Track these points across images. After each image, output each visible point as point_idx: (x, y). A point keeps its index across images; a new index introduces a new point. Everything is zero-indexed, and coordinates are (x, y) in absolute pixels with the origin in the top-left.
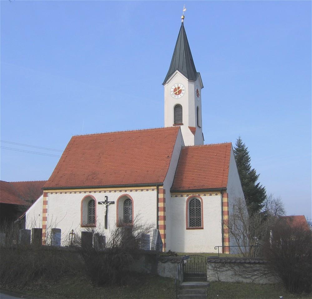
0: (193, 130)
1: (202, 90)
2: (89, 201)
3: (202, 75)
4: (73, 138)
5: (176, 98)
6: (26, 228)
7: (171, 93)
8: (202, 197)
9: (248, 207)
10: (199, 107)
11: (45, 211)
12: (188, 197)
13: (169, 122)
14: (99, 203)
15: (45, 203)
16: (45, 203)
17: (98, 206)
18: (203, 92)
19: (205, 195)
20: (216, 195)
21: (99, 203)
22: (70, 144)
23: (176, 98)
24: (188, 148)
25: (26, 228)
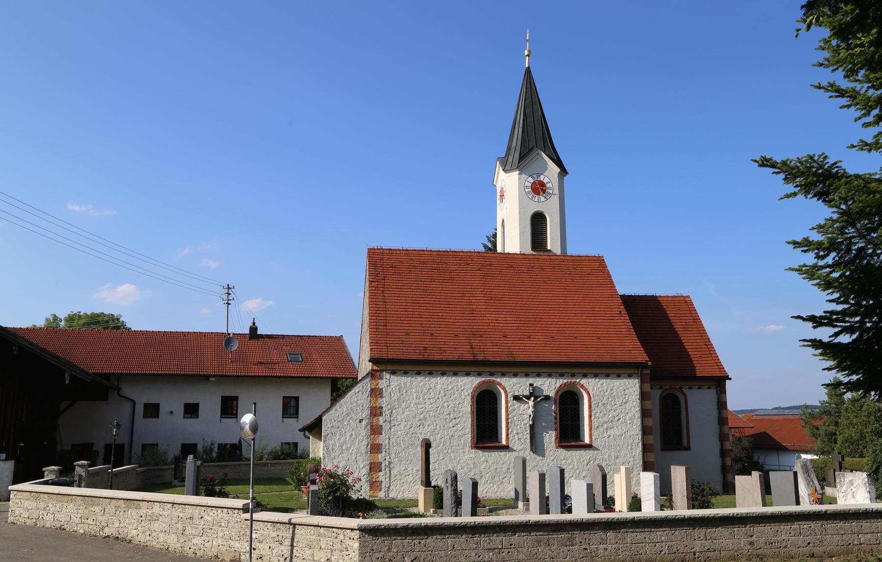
7: (527, 190)
14: (516, 398)
19: (690, 388)
20: (709, 388)
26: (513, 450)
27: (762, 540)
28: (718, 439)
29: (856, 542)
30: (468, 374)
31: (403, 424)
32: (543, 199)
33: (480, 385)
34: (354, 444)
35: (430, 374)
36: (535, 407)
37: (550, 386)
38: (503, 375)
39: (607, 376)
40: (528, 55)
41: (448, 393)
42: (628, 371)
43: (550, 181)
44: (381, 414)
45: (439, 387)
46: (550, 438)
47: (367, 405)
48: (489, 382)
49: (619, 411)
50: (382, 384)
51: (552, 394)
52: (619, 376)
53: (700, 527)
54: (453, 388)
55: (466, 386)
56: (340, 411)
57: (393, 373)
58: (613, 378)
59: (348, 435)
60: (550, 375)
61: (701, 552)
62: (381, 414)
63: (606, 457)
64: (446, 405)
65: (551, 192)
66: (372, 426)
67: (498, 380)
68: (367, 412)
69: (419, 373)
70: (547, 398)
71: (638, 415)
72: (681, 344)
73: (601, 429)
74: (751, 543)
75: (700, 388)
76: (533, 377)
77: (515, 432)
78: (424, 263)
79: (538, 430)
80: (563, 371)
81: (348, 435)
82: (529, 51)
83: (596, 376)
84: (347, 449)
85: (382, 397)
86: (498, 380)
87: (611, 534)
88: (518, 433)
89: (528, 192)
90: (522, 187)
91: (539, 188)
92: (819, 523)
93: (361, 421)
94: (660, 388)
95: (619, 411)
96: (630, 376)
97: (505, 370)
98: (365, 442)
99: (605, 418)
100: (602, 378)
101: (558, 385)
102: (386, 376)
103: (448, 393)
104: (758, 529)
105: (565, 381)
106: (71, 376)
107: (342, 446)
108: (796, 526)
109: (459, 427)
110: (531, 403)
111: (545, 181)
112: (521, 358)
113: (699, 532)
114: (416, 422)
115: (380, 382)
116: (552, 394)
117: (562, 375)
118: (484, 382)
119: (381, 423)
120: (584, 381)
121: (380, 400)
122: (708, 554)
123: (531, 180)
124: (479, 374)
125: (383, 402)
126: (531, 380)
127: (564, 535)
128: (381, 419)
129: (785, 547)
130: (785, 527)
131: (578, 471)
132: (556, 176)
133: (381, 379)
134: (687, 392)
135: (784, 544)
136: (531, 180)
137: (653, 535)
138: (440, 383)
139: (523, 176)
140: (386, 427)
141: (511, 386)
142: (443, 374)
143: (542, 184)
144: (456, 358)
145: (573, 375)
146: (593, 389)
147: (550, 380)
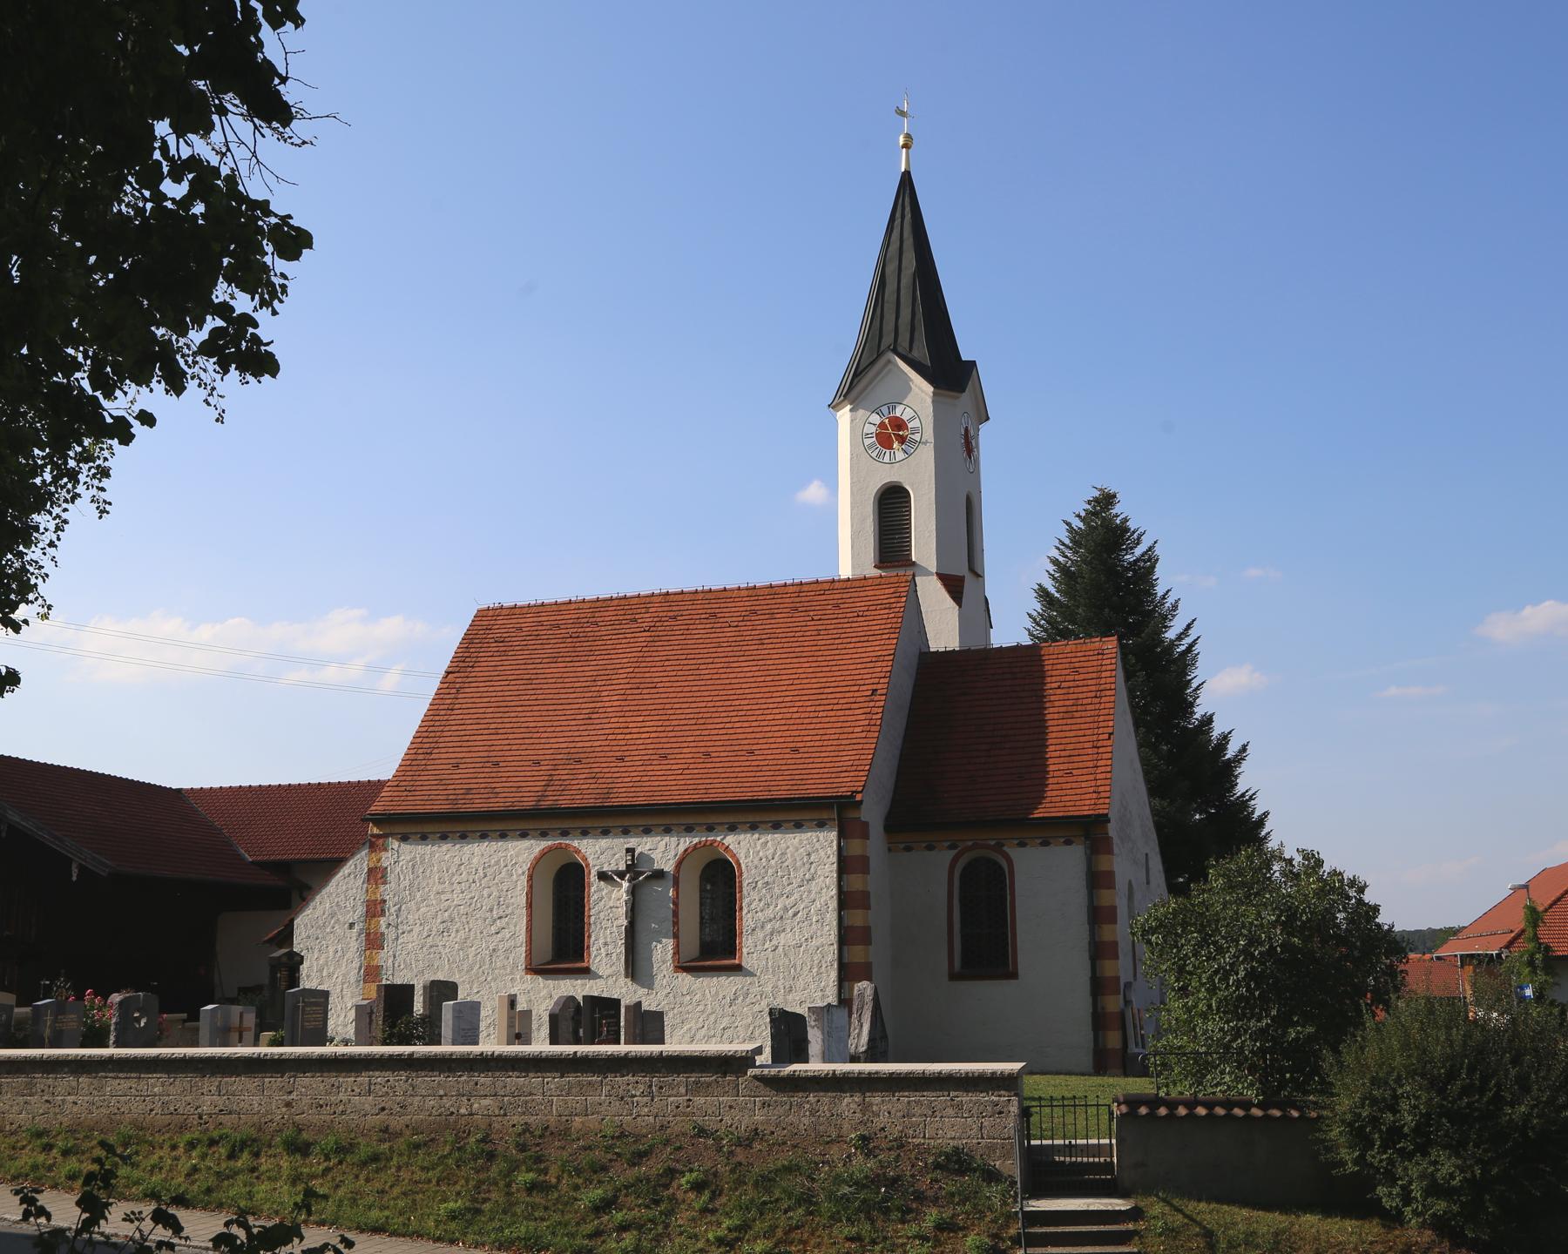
0: (953, 586)
1: (984, 428)
2: (552, 876)
3: (987, 376)
4: (482, 615)
5: (887, 459)
6: (1111, 644)
7: (868, 442)
8: (1016, 853)
9: (1157, 802)
10: (974, 500)
11: (375, 909)
12: (954, 852)
13: (849, 555)
14: (603, 876)
15: (376, 875)
16: (376, 875)
17: (595, 888)
18: (987, 436)
19: (1022, 845)
20: (1068, 842)
21: (603, 876)
22: (469, 640)
23: (887, 459)
24: (945, 658)
25: (1111, 644)
26: (597, 976)
27: (306, 1100)
28: (1086, 956)
29: (463, 1111)
30: (524, 835)
31: (417, 929)
32: (900, 455)
33: (544, 854)
34: (340, 966)
35: (463, 837)
36: (633, 892)
37: (664, 850)
38: (585, 833)
39: (776, 827)
40: (906, 146)
41: (490, 871)
42: (816, 815)
43: (917, 415)
44: (383, 913)
45: (475, 860)
46: (662, 952)
47: (362, 896)
48: (559, 847)
49: (796, 896)
50: (387, 859)
51: (669, 867)
52: (798, 826)
53: (213, 1074)
54: (497, 863)
55: (522, 852)
56: (319, 912)
57: (404, 838)
58: (788, 831)
59: (331, 950)
60: (667, 831)
61: (210, 1115)
62: (383, 913)
63: (769, 989)
64: (485, 893)
65: (917, 437)
66: (368, 935)
67: (575, 843)
68: (361, 910)
69: (444, 837)
70: (659, 875)
71: (834, 904)
72: (1042, 745)
73: (760, 934)
74: (288, 1105)
75: (1045, 843)
76: (637, 835)
77: (601, 941)
78: (558, 626)
79: (642, 937)
80: (690, 820)
81: (331, 950)
82: (908, 136)
83: (753, 827)
84: (330, 976)
85: (385, 883)
86: (575, 843)
87: (84, 1080)
88: (606, 944)
89: (870, 446)
90: (857, 436)
91: (892, 434)
92: (403, 1075)
93: (351, 926)
94: (952, 847)
95: (796, 896)
96: (821, 825)
97: (588, 824)
98: (356, 964)
99: (769, 912)
100: (766, 831)
101: (681, 849)
102: (394, 844)
103: (490, 871)
104: (304, 1080)
105: (696, 840)
106: (82, 868)
107: (321, 971)
108: (363, 1079)
109: (506, 934)
110: (625, 884)
111: (905, 418)
112: (621, 798)
113: (210, 1083)
114: (436, 925)
115: (384, 855)
116: (669, 867)
117: (689, 829)
118: (550, 850)
119: (383, 929)
120: (730, 840)
121: (382, 888)
122: (222, 1118)
123: (876, 419)
124: (544, 834)
125: (387, 892)
126: (632, 842)
127: (22, 1079)
128: (383, 921)
129: (343, 1113)
130: (348, 1081)
131: (712, 1018)
132: (929, 401)
133: (386, 850)
134: (1016, 853)
135: (341, 1108)
136: (876, 419)
137: (142, 1085)
138: (479, 853)
139: (861, 412)
140: (390, 934)
141: (600, 852)
142: (484, 836)
143: (899, 424)
144: (590, 801)
145: (710, 829)
146: (747, 849)
147: (667, 839)
